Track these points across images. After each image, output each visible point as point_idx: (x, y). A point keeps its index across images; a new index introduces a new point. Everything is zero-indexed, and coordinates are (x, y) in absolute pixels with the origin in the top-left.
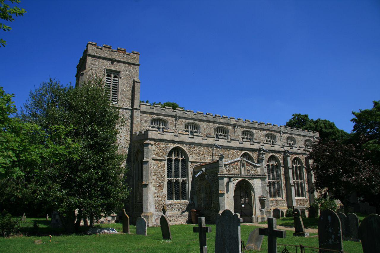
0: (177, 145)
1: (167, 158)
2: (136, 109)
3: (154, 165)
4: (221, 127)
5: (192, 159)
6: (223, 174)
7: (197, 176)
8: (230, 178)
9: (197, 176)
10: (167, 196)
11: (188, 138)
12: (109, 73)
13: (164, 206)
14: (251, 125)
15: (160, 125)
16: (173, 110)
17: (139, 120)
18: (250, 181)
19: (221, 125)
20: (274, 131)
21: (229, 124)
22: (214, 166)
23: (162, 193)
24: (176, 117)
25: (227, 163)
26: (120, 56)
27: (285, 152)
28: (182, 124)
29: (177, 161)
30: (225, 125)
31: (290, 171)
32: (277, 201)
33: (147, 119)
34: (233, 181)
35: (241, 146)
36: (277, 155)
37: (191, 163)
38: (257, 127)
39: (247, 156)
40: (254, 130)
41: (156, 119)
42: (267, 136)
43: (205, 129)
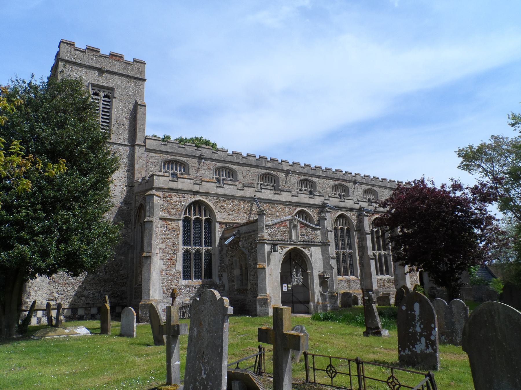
0: (198, 198)
1: (183, 216)
2: (140, 146)
3: (161, 227)
4: (269, 174)
5: (221, 218)
6: (263, 240)
7: (226, 243)
8: (274, 245)
9: (226, 243)
10: (182, 274)
11: (215, 188)
12: (96, 90)
13: (173, 290)
14: (311, 172)
15: (176, 170)
16: (196, 148)
17: (145, 162)
18: (304, 250)
19: (268, 171)
20: (346, 181)
21: (279, 169)
22: (252, 227)
23: (174, 270)
24: (200, 158)
25: (270, 223)
26: (114, 65)
27: (361, 209)
28: (209, 169)
29: (198, 221)
30: (274, 171)
31: (369, 237)
32: (349, 281)
33: (156, 160)
34: (279, 251)
35: (295, 200)
36: (348, 214)
37: (220, 224)
38: (321, 174)
39: (305, 216)
40: (317, 179)
41: (170, 161)
42: (335, 187)
43: (244, 177)
